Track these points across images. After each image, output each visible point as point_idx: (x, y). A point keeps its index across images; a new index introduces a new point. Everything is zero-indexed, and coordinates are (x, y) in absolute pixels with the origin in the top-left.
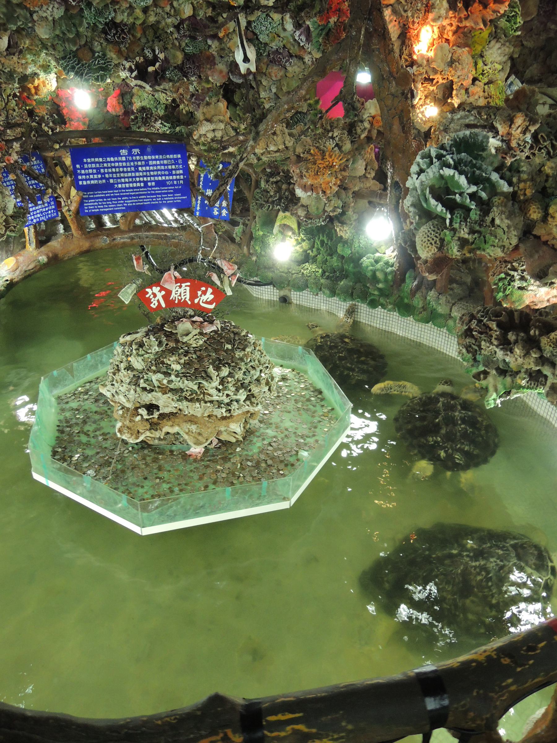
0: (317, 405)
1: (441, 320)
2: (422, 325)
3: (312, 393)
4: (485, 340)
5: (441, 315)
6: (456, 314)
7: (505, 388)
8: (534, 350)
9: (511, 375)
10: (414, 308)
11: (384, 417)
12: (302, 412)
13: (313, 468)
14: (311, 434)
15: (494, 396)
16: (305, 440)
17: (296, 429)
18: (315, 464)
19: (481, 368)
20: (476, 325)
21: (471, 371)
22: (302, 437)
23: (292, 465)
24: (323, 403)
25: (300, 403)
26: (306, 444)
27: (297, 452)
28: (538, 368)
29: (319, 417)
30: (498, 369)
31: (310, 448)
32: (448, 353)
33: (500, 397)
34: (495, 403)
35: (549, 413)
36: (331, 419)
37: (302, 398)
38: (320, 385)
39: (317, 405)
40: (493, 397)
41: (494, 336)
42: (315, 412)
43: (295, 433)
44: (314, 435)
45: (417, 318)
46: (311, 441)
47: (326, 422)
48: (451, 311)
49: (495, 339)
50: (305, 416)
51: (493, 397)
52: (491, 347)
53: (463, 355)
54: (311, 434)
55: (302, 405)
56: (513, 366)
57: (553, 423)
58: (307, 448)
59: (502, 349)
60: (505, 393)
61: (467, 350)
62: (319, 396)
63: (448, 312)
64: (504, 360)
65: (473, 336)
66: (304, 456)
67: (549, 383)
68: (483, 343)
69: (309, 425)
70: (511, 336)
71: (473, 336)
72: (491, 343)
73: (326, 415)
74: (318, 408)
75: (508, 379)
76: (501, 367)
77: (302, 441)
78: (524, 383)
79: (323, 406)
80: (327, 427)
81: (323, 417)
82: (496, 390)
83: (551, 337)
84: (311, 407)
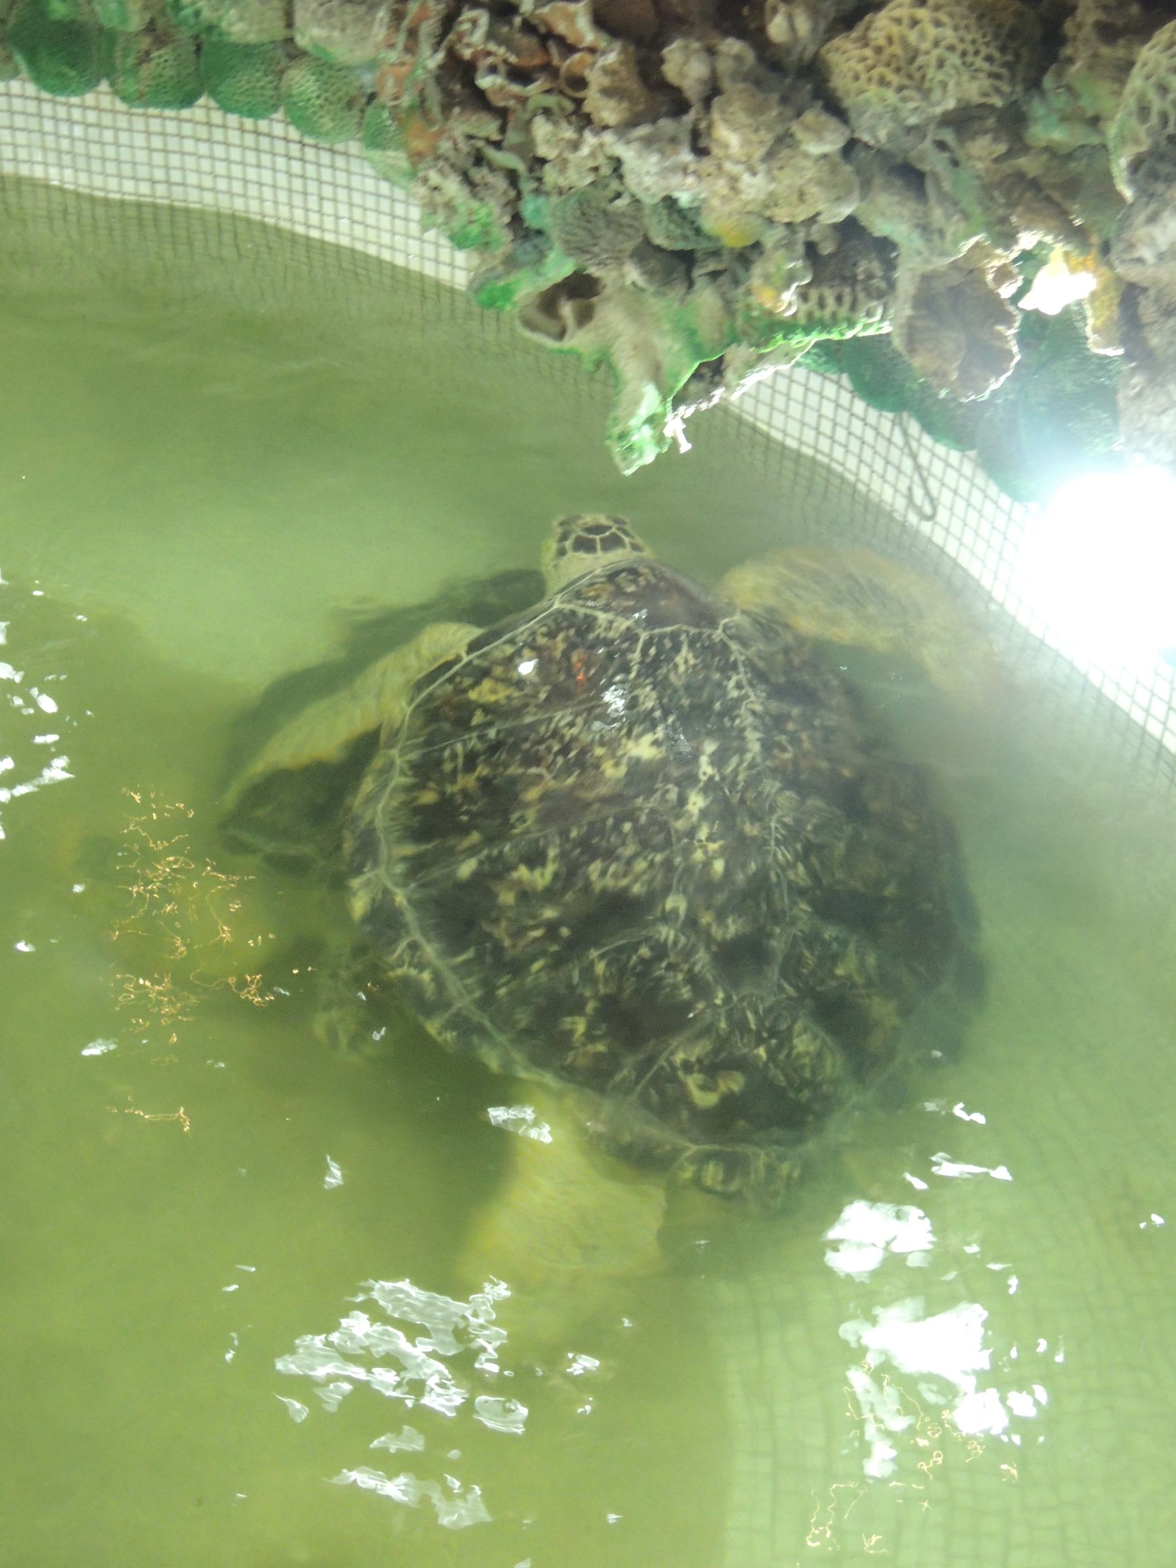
1: (249, 79)
2: (165, 122)
4: (547, 112)
5: (247, 52)
6: (317, 32)
8: (809, 117)
9: (714, 275)
10: (109, 36)
11: (1059, 1358)
15: (650, 399)
19: (559, 267)
20: (491, 35)
21: (507, 292)
28: (845, 211)
30: (646, 252)
33: (678, 401)
34: (660, 439)
40: (644, 412)
41: (596, 79)
45: (131, 88)
48: (290, 25)
49: (607, 92)
51: (644, 412)
52: (590, 139)
56: (723, 223)
59: (648, 142)
60: (697, 376)
61: (467, 179)
63: (277, 30)
64: (670, 202)
65: (480, 100)
67: (905, 279)
68: (542, 129)
70: (684, 64)
71: (480, 100)
72: (584, 121)
75: (706, 298)
76: (659, 240)
78: (788, 302)
82: (657, 374)
83: (878, 36)
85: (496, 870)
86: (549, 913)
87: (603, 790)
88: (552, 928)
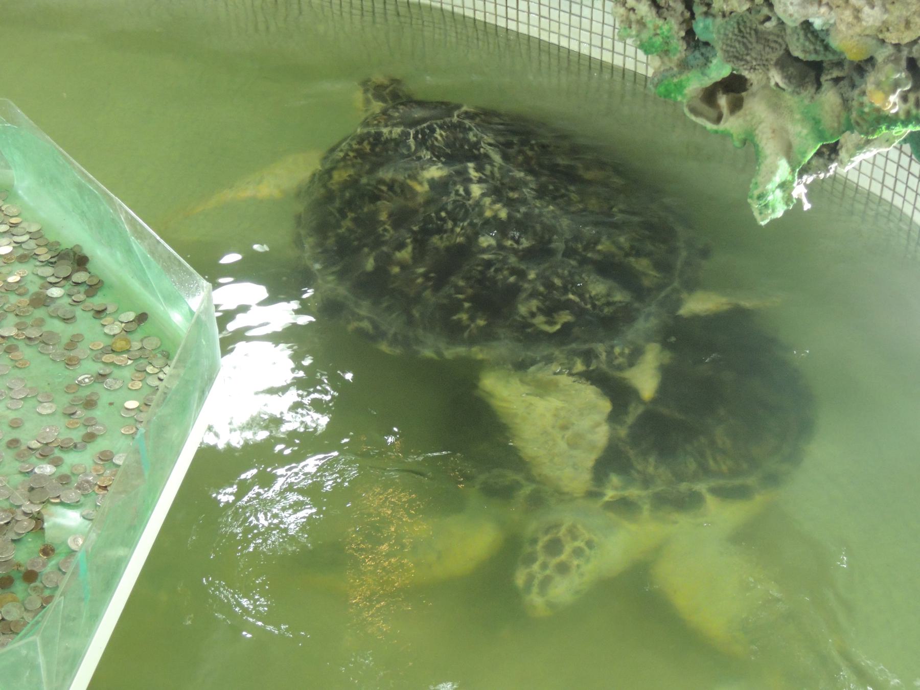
0: (78, 312)
3: (48, 271)
7: (820, 135)
12: (27, 352)
13: (110, 576)
14: (77, 435)
15: (783, 170)
16: (57, 462)
17: (15, 425)
18: (121, 552)
19: (719, 70)
21: (680, 87)
22: (44, 454)
23: (30, 576)
24: (98, 301)
25: (11, 319)
26: (64, 480)
27: (38, 519)
29: (96, 359)
30: (787, 61)
31: (84, 491)
32: (512, 26)
33: (804, 170)
34: (788, 199)
35: (889, 182)
36: (142, 356)
37: (13, 299)
38: (75, 233)
39: (78, 312)
40: (778, 179)
42: (73, 344)
43: (13, 443)
44: (90, 437)
46: (80, 461)
47: (127, 373)
50: (40, 367)
51: (778, 179)
53: (641, 23)
54: (77, 435)
55: (20, 327)
57: (908, 209)
58: (72, 495)
60: (819, 154)
62: (80, 277)
64: (807, 25)
66: (69, 531)
69: (65, 399)
73: (120, 344)
74: (85, 324)
75: (830, 97)
76: (797, 53)
77: (48, 469)
78: (893, 104)
79: (99, 313)
80: (133, 393)
81: (108, 358)
82: (789, 152)
84: (56, 326)
85: (384, 262)
86: (421, 270)
87: (420, 200)
88: (425, 275)
